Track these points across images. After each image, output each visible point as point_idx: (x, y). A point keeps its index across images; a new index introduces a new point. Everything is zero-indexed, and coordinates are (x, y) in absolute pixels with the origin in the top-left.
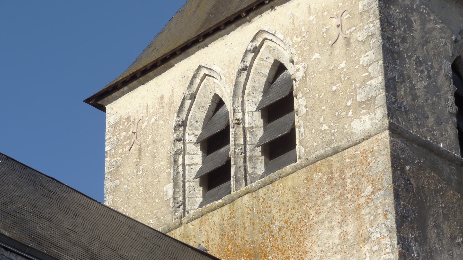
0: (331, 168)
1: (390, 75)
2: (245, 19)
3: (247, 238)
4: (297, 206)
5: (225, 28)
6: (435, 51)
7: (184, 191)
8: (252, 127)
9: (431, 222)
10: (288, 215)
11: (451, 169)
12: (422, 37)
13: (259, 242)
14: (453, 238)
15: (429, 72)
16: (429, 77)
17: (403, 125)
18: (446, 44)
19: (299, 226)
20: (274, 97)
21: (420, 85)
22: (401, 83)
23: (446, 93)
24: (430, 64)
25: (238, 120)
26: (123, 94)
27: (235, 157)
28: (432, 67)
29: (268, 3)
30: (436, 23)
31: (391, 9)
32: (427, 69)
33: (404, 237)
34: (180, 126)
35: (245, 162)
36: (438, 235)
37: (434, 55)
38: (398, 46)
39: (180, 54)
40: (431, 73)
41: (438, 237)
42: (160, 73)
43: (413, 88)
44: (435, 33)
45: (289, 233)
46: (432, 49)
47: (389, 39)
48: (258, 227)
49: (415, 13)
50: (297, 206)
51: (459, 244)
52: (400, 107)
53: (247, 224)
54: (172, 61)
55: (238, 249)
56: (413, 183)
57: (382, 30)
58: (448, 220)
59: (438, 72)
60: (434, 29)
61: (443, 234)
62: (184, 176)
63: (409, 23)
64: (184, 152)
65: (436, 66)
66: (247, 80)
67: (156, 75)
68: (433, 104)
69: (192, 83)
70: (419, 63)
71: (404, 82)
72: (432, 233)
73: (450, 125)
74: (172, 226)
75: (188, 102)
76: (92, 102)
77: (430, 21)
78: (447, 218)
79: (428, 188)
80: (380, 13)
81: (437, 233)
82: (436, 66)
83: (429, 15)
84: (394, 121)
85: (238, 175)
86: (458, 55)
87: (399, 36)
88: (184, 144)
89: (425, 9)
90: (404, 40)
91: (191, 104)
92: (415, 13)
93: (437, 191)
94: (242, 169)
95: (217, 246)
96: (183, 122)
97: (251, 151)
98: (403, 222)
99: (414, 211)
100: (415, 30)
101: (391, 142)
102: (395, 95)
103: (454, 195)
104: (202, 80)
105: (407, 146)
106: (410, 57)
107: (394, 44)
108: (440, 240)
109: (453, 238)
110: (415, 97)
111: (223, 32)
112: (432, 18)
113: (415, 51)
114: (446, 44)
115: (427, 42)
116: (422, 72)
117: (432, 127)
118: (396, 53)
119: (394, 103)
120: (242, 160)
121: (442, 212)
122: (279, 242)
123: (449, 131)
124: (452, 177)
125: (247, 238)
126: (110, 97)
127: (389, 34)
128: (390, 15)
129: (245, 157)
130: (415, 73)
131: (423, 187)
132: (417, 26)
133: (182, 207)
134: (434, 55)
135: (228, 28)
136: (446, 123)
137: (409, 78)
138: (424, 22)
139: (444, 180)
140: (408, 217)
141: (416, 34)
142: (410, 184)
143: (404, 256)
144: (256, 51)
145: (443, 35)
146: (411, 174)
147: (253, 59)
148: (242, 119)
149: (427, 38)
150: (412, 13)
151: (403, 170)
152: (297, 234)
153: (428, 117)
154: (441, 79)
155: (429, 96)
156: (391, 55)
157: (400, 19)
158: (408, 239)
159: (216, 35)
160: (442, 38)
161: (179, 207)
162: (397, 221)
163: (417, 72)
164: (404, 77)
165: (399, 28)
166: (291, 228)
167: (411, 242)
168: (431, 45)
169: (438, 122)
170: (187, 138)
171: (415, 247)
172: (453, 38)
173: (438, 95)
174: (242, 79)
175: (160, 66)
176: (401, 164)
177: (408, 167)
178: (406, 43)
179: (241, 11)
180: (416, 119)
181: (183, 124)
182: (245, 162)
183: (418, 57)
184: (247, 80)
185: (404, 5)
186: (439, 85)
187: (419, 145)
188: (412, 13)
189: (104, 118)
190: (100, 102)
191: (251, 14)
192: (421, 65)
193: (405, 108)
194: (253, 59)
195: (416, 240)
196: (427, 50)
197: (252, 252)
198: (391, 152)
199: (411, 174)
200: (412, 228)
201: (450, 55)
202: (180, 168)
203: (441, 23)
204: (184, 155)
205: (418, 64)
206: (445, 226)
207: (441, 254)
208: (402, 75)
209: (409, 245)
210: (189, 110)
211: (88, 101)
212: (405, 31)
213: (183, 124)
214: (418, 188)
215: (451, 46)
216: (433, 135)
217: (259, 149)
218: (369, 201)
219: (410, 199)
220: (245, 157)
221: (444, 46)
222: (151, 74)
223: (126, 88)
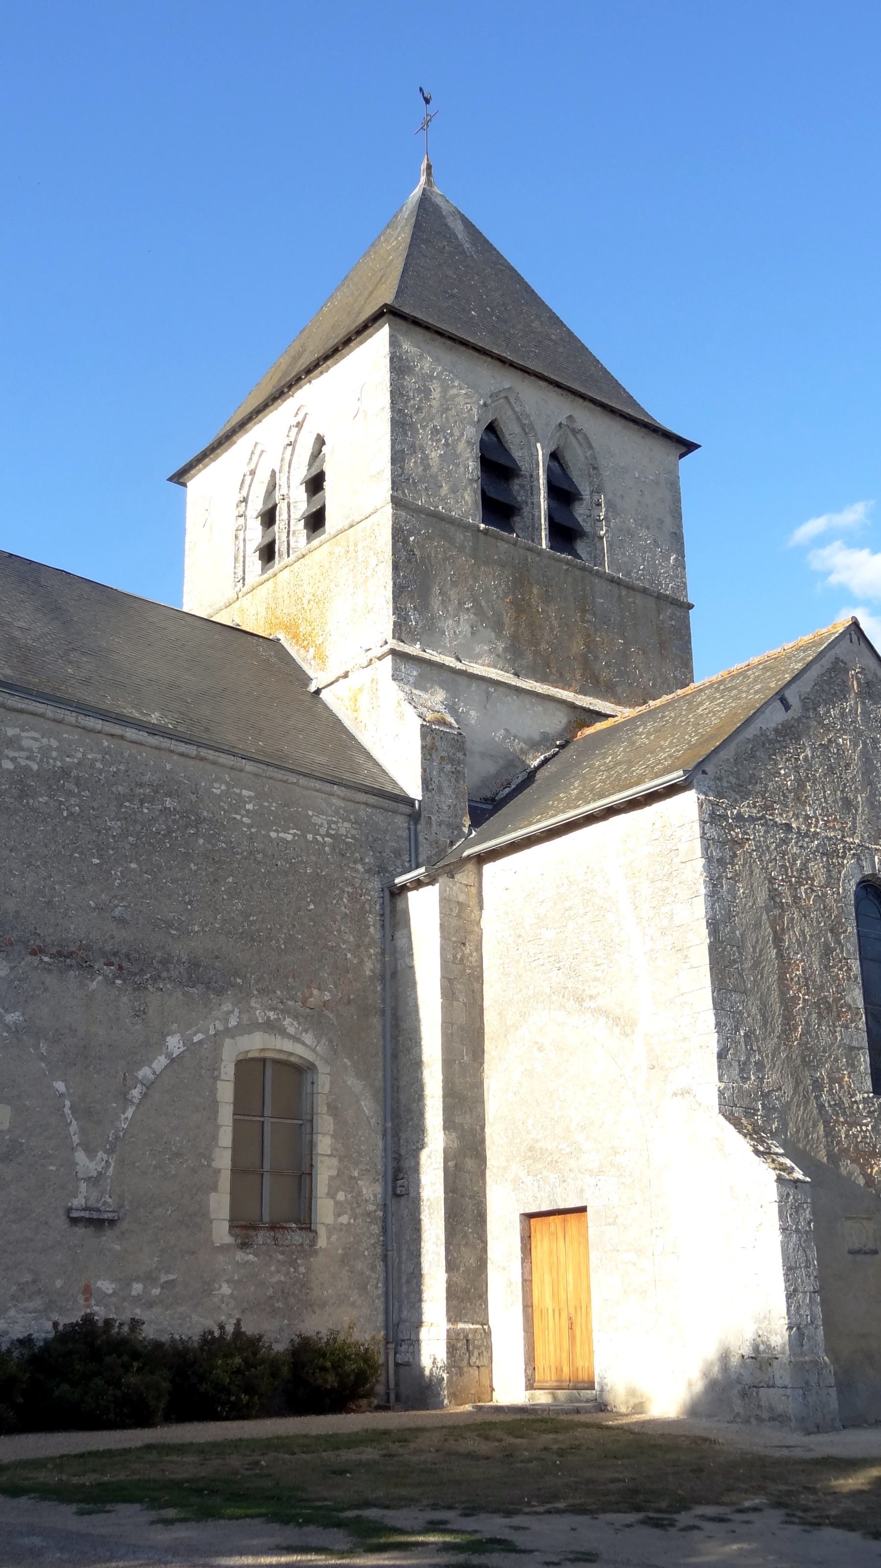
0: (347, 542)
1: (398, 447)
2: (287, 395)
3: (285, 611)
4: (322, 579)
5: (273, 404)
6: (457, 417)
7: (244, 566)
8: (296, 502)
9: (436, 590)
10: (315, 587)
11: (465, 536)
12: (442, 405)
13: (293, 615)
14: (461, 604)
15: (447, 440)
16: (447, 445)
17: (410, 497)
18: (471, 409)
19: (323, 599)
20: (314, 472)
21: (434, 455)
22: (411, 454)
23: (467, 459)
24: (449, 431)
25: (283, 495)
26: (200, 471)
27: (279, 532)
28: (452, 434)
29: (305, 377)
30: (461, 389)
31: (405, 379)
32: (445, 437)
33: (400, 607)
34: (241, 502)
35: (288, 536)
36: (443, 601)
37: (455, 422)
38: (411, 417)
39: (240, 430)
40: (450, 441)
41: (442, 604)
42: (226, 450)
43: (426, 457)
44: (460, 399)
45: (315, 604)
46: (454, 416)
47: (400, 411)
48: (293, 599)
49: (434, 381)
50: (322, 579)
51: (468, 609)
52: (408, 479)
53: (286, 597)
54: (234, 438)
55: (278, 621)
56: (416, 553)
57: (392, 403)
58: (457, 587)
59: (459, 439)
60: (458, 395)
61: (450, 601)
62: (244, 552)
63: (427, 392)
64: (246, 528)
65: (457, 433)
66: (292, 455)
67: (223, 452)
68: (450, 472)
69: (251, 459)
70: (435, 431)
71: (415, 453)
72: (436, 602)
73: (469, 492)
74: (231, 601)
75: (248, 479)
76: (175, 480)
77: (454, 387)
78: (454, 584)
79: (435, 556)
80: (391, 385)
81: (443, 600)
82: (457, 433)
83: (453, 381)
84: (400, 494)
85: (281, 549)
86: (494, 418)
87: (413, 407)
88: (246, 520)
89: (448, 376)
90: (419, 410)
91: (252, 480)
92: (434, 381)
93: (445, 559)
94: (286, 543)
95: (263, 619)
96: (244, 498)
97: (294, 525)
98: (402, 592)
99: (415, 581)
100: (434, 399)
101: (394, 515)
102: (402, 468)
103: (466, 561)
104: (260, 456)
105: (413, 517)
106: (423, 428)
107: (406, 415)
108: (445, 606)
109: (461, 604)
110: (427, 467)
111: (271, 408)
112: (456, 384)
113: (431, 420)
114: (471, 409)
115: (448, 409)
116: (440, 440)
117: (446, 495)
118: (407, 424)
119: (401, 475)
120: (286, 535)
121: (451, 579)
122: (308, 614)
123: (467, 497)
124: (466, 543)
125: (285, 611)
126: (189, 475)
127: (400, 406)
128: (403, 386)
129: (289, 532)
130: (430, 443)
131: (429, 557)
132: (436, 394)
133: (241, 581)
134: (455, 422)
135: (276, 404)
136: (463, 490)
137: (422, 449)
138: (445, 389)
139: (456, 547)
140: (408, 587)
141: (434, 403)
142: (414, 554)
143: (400, 625)
144: (299, 425)
145: (468, 401)
146: (415, 545)
147: (298, 433)
148: (287, 494)
149: (449, 405)
150: (431, 381)
151: (406, 541)
152: (321, 606)
153: (442, 486)
154: (461, 446)
155: (445, 464)
156: (401, 428)
157: (416, 389)
158: (406, 609)
159: (267, 411)
160: (468, 403)
161: (239, 581)
162: (393, 592)
163: (432, 441)
164: (415, 447)
165: (414, 398)
166: (317, 600)
167: (409, 612)
168: (453, 412)
169: (454, 490)
170: (248, 513)
171: (413, 617)
172: (481, 402)
173: (456, 463)
174: (287, 456)
175: (224, 443)
176: (404, 536)
177: (412, 539)
178: (422, 413)
179: (283, 386)
180: (426, 489)
181: (245, 500)
182: (288, 536)
183: (435, 426)
184: (292, 455)
185: (422, 374)
186: (458, 452)
187: (428, 515)
188: (431, 381)
189: (185, 494)
190: (181, 480)
191: (293, 390)
192: (438, 434)
193: (414, 480)
194: (298, 433)
195: (415, 609)
196: (447, 418)
197: (288, 624)
198: (393, 525)
199: (415, 545)
200: (412, 598)
201: (476, 420)
202: (241, 545)
203: (468, 388)
204: (245, 530)
205: (435, 433)
206: (453, 594)
207: (445, 620)
208: (413, 446)
209: (407, 614)
210: (250, 486)
211: (170, 479)
212: (421, 400)
213: (245, 500)
214: (421, 557)
215: (478, 411)
216: (446, 503)
217: (303, 522)
218: (374, 573)
219: (412, 569)
220: (289, 532)
221: (468, 411)
222: (219, 451)
223: (201, 466)
